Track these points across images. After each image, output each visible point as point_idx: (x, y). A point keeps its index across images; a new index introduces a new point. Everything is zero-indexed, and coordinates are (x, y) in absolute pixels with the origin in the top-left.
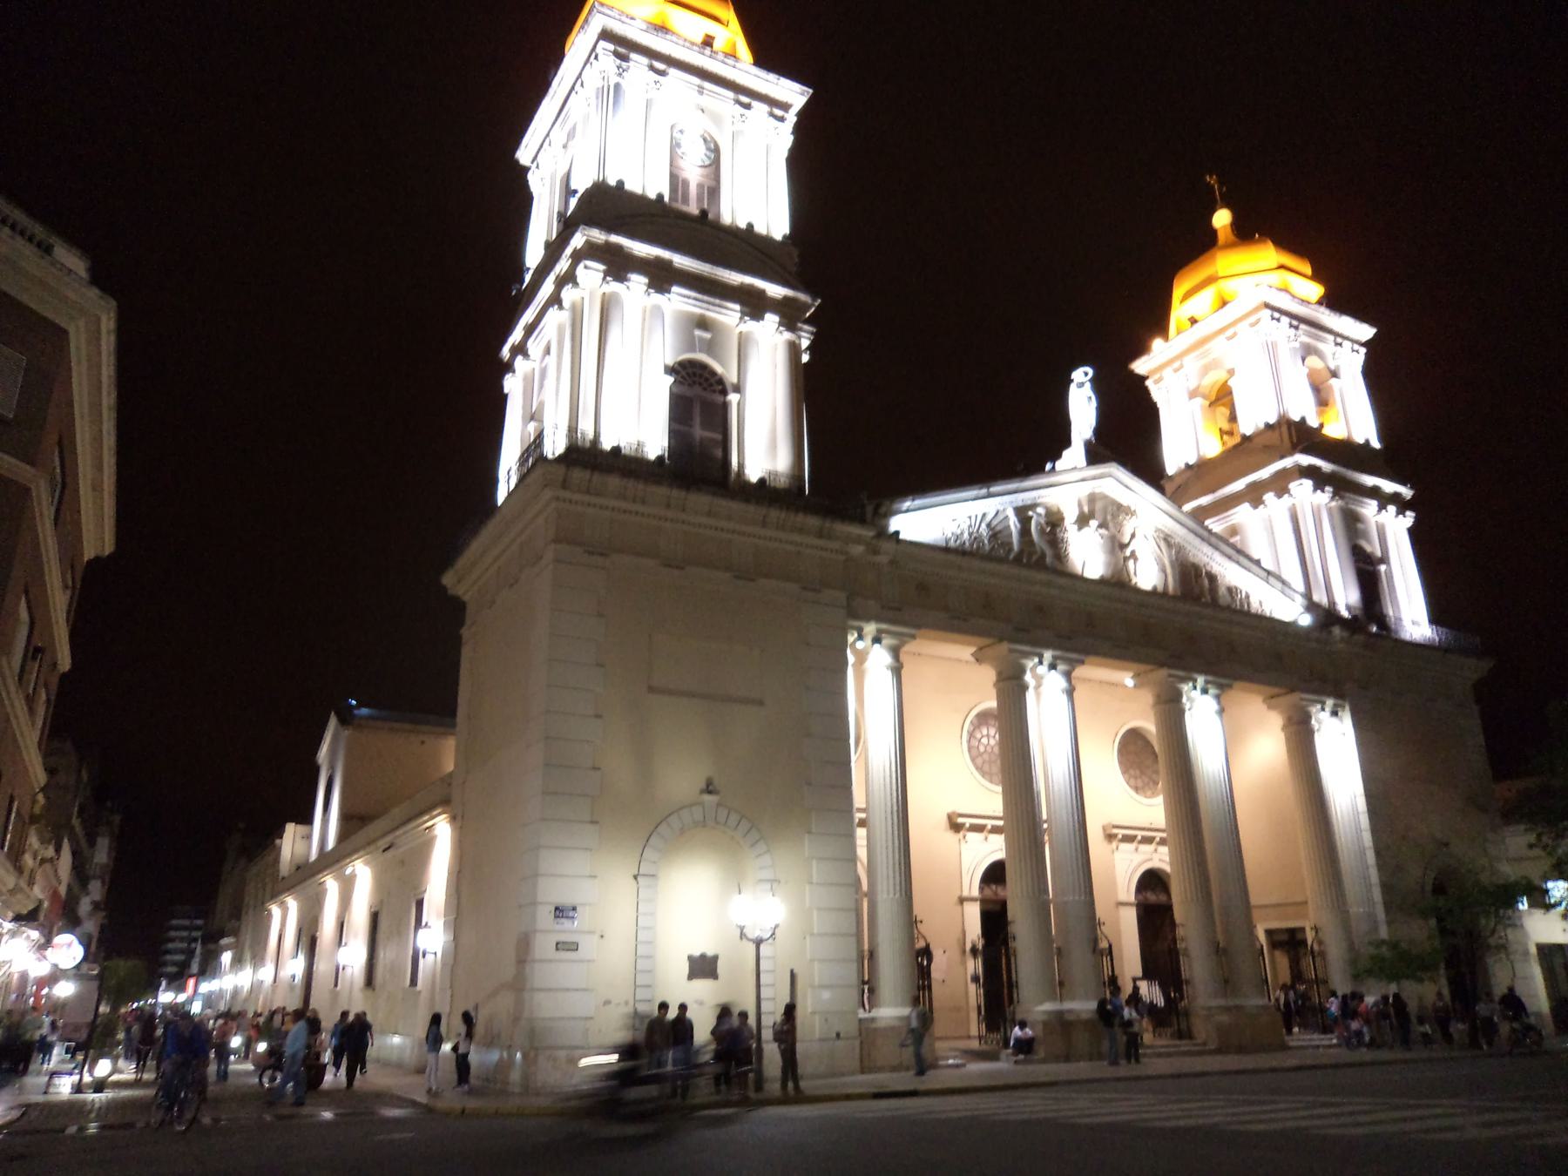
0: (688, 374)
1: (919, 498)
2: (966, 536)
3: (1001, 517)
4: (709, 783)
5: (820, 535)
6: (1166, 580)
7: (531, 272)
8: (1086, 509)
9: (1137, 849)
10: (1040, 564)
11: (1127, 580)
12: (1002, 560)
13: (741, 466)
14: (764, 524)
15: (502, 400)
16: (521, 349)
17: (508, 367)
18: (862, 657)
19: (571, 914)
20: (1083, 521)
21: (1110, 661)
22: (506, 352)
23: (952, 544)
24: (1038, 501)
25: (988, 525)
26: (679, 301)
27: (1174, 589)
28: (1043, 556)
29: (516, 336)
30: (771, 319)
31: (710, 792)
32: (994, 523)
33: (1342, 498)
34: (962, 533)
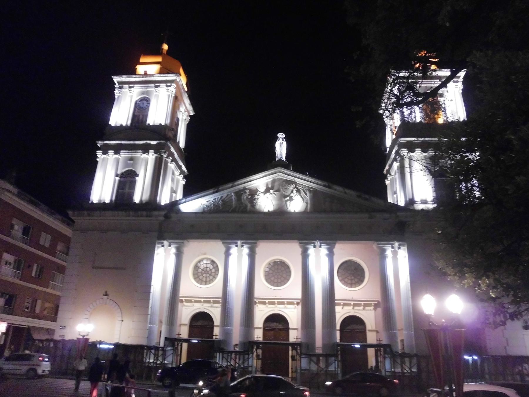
0: (125, 176)
1: (189, 197)
2: (212, 205)
3: (229, 196)
4: (106, 292)
5: (147, 216)
6: (307, 206)
7: (388, 148)
8: (270, 186)
9: (343, 308)
10: (244, 211)
11: (287, 208)
12: (228, 212)
13: (160, 200)
14: (129, 216)
15: (386, 186)
16: (388, 172)
17: (385, 177)
18: (395, 254)
19: (64, 328)
20: (267, 191)
21: (291, 241)
22: (385, 172)
23: (206, 210)
24: (247, 187)
25: (222, 201)
26: (124, 155)
27: (310, 209)
28: (246, 206)
29: (387, 167)
30: (151, 152)
31: (106, 295)
32: (225, 199)
33: (425, 152)
34: (211, 205)
